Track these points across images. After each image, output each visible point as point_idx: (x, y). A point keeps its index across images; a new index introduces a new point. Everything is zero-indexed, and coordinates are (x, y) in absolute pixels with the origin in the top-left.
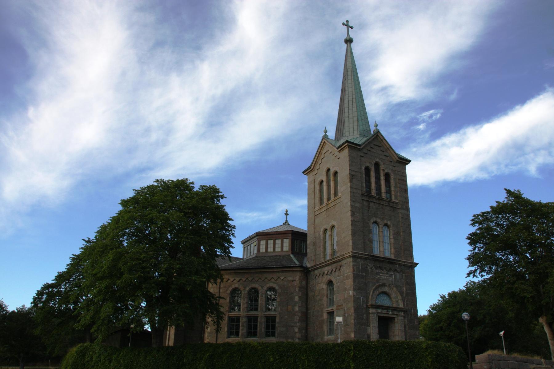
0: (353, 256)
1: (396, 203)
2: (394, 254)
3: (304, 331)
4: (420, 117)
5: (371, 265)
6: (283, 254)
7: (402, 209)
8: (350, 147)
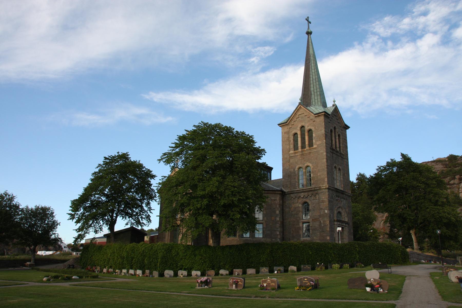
0: (328, 189)
1: (343, 155)
2: (343, 188)
3: (282, 234)
5: (335, 194)
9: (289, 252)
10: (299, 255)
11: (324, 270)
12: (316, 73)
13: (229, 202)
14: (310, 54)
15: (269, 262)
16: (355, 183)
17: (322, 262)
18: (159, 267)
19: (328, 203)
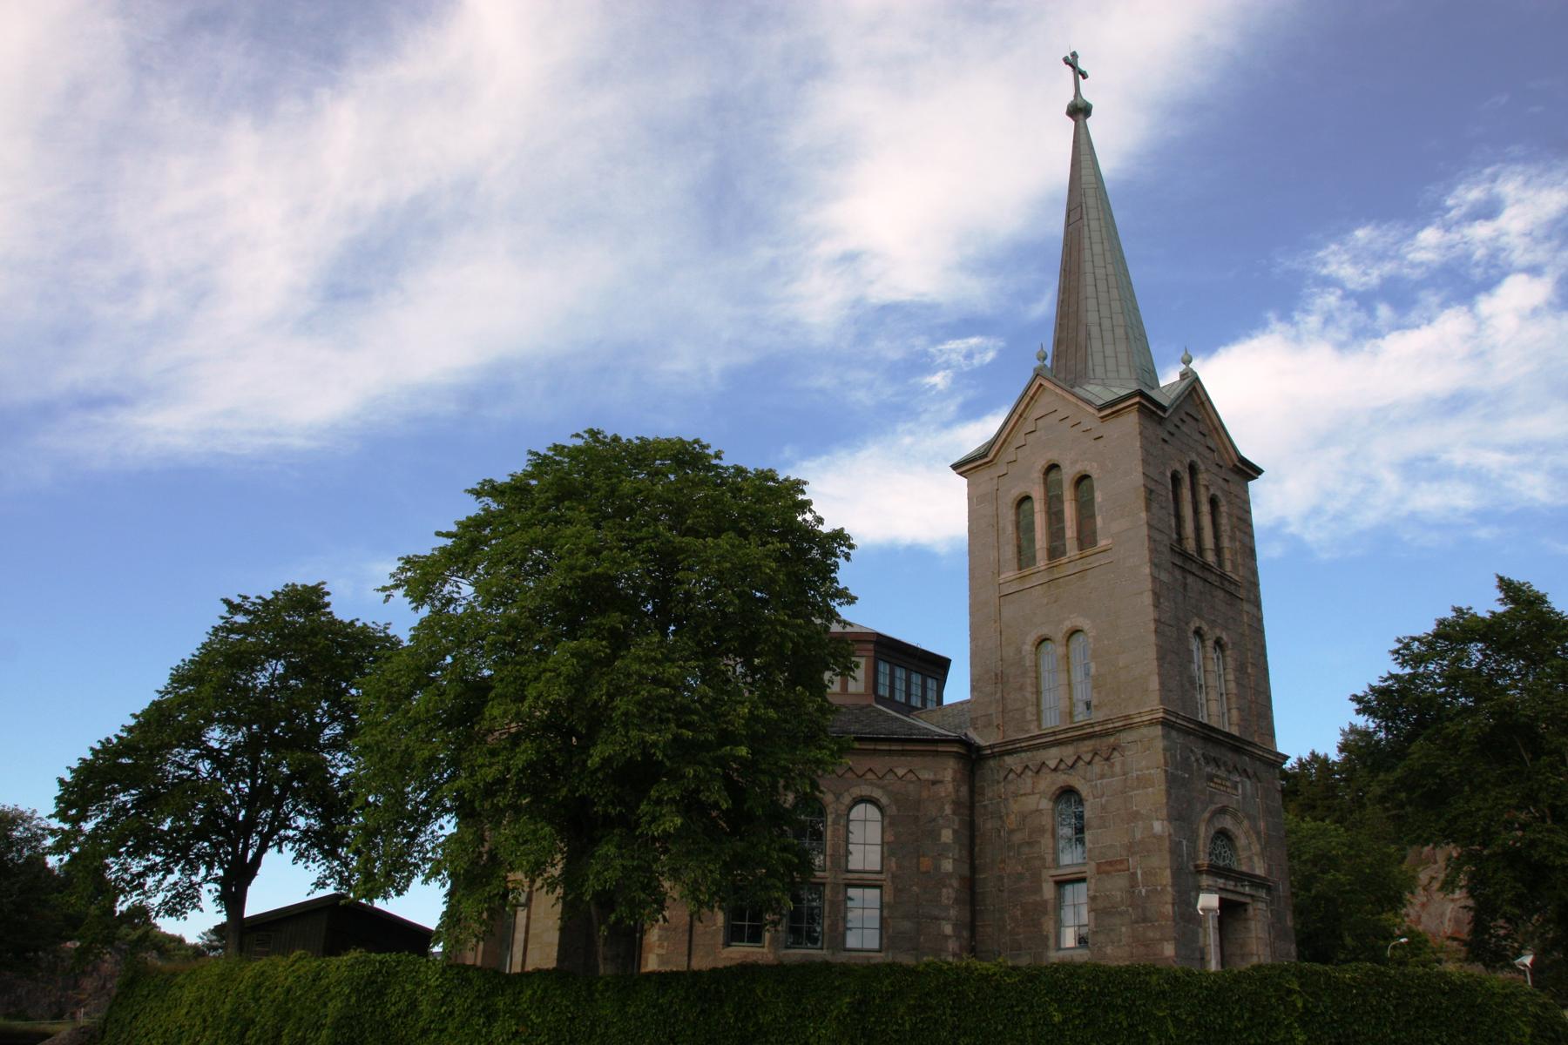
0: (1165, 723)
1: (1235, 583)
2: (1238, 725)
3: (965, 934)
4: (940, 351)
5: (1199, 752)
6: (848, 701)
7: (1248, 601)
8: (1142, 409)
9: (948, 1011)
12: (1108, 255)
14: (1083, 186)
16: (1334, 762)
19: (1163, 787)
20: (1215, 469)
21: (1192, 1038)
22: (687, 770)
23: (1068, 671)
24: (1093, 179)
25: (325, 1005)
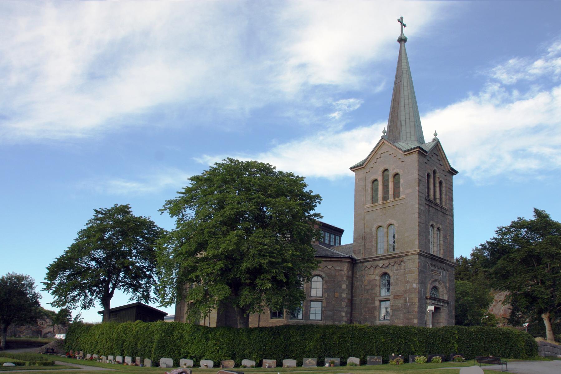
0: (420, 254)
1: (445, 209)
2: (443, 254)
3: (349, 316)
5: (429, 263)
9: (350, 338)
10: (366, 343)
11: (402, 364)
12: (410, 95)
13: (254, 266)
14: (402, 69)
15: (319, 350)
17: (400, 353)
18: (155, 354)
19: (417, 274)
20: (442, 172)
21: (424, 346)
22: (273, 270)
23: (388, 237)
24: (406, 67)
25: (153, 336)
